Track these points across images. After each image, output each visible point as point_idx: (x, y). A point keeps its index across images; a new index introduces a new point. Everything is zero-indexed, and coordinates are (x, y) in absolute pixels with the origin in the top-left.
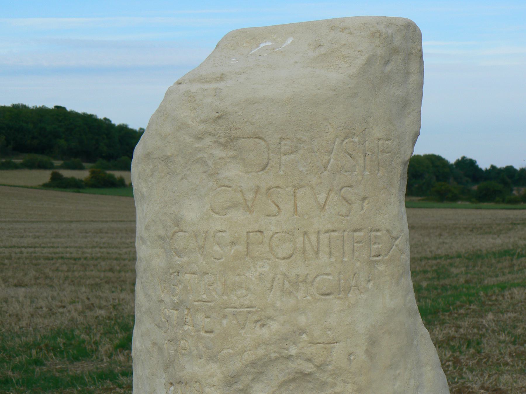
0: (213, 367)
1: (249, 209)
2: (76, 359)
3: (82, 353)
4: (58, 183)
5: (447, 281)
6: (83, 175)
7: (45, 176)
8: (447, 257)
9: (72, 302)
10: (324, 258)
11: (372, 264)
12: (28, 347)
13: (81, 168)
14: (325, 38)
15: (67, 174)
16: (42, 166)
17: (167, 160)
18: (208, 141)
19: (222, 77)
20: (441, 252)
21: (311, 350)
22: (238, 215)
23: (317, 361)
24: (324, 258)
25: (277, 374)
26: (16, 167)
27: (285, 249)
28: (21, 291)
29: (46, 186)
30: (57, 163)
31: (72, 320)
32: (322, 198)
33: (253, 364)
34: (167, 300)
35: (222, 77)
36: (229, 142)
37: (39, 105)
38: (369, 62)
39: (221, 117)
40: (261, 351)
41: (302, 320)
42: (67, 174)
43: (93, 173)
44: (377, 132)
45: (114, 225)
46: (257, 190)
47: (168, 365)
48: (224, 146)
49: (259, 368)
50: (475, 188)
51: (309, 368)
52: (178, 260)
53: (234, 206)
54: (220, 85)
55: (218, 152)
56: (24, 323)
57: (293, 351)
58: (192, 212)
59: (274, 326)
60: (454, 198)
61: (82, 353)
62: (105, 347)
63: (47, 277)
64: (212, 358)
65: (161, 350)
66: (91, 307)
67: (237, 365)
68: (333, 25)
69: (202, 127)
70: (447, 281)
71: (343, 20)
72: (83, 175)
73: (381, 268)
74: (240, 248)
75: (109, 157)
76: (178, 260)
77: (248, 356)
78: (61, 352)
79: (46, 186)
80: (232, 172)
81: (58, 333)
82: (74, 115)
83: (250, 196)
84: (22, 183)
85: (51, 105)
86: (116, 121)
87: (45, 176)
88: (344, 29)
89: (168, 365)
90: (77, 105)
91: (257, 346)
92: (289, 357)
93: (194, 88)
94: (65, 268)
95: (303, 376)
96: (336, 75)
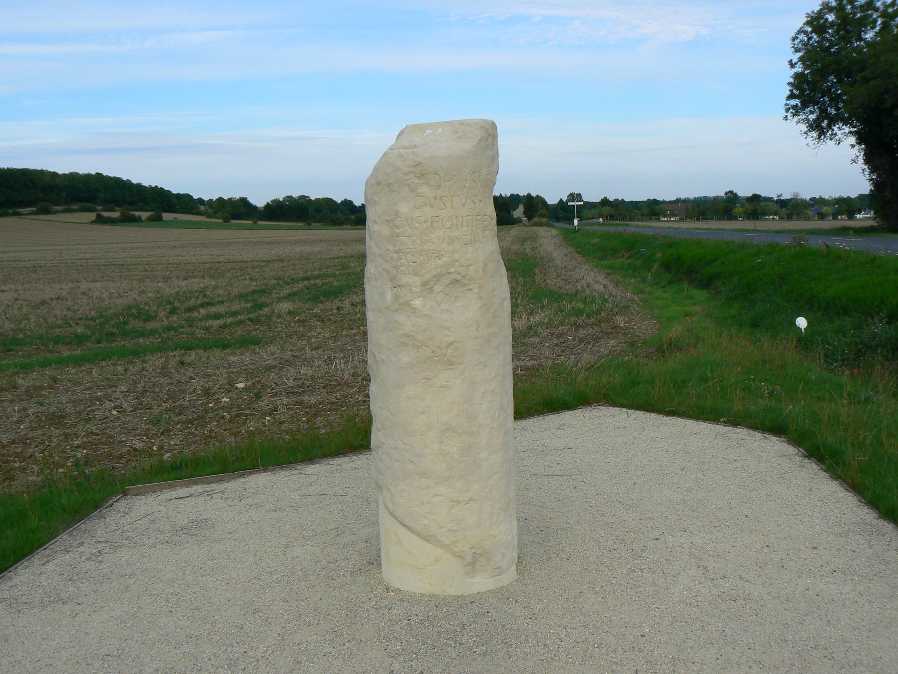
0: (416, 278)
1: (431, 206)
2: (148, 320)
3: (149, 318)
4: (100, 220)
5: (350, 270)
6: (116, 214)
7: (92, 216)
8: (345, 257)
9: (131, 290)
10: (465, 228)
11: (484, 230)
12: (117, 315)
13: (114, 211)
14: (459, 128)
15: (106, 214)
16: (90, 210)
17: (389, 185)
18: (411, 176)
19: (415, 147)
20: (341, 254)
21: (460, 269)
22: (426, 209)
23: (463, 274)
24: (465, 228)
25: (445, 280)
26: (74, 211)
27: (448, 224)
28: (98, 284)
29: (93, 222)
30: (99, 208)
31: (135, 299)
32: (464, 201)
33: (435, 276)
34: (391, 249)
35: (415, 147)
36: (422, 176)
37: (86, 172)
38: (481, 140)
39: (418, 164)
40: (439, 270)
41: (457, 256)
42: (106, 214)
43: (121, 213)
44: (485, 171)
45: (140, 244)
46: (435, 198)
47: (393, 279)
48: (419, 178)
49: (437, 277)
50: (353, 217)
51: (459, 277)
52: (398, 231)
53: (425, 205)
54: (415, 150)
55: (416, 181)
56: (106, 302)
57: (453, 270)
58: (404, 208)
59: (445, 259)
60: (342, 224)
61: (149, 318)
62: (162, 314)
63: (109, 276)
64: (416, 274)
65: (388, 272)
66: (143, 292)
67: (428, 276)
68: (461, 123)
69: (408, 169)
70: (350, 270)
71: (466, 121)
72: (116, 214)
73: (488, 232)
74: (429, 224)
75: (131, 204)
76: (398, 231)
77: (433, 273)
78: (138, 317)
79: (93, 222)
80: (424, 189)
81: (130, 307)
82: (108, 178)
83: (432, 200)
84: (69, 220)
85: (93, 173)
86: (135, 181)
87: (92, 216)
88: (468, 125)
89: (393, 279)
90: (110, 172)
91: (437, 268)
92: (450, 273)
93: (402, 151)
94: (117, 270)
95: (457, 281)
96: (468, 145)
